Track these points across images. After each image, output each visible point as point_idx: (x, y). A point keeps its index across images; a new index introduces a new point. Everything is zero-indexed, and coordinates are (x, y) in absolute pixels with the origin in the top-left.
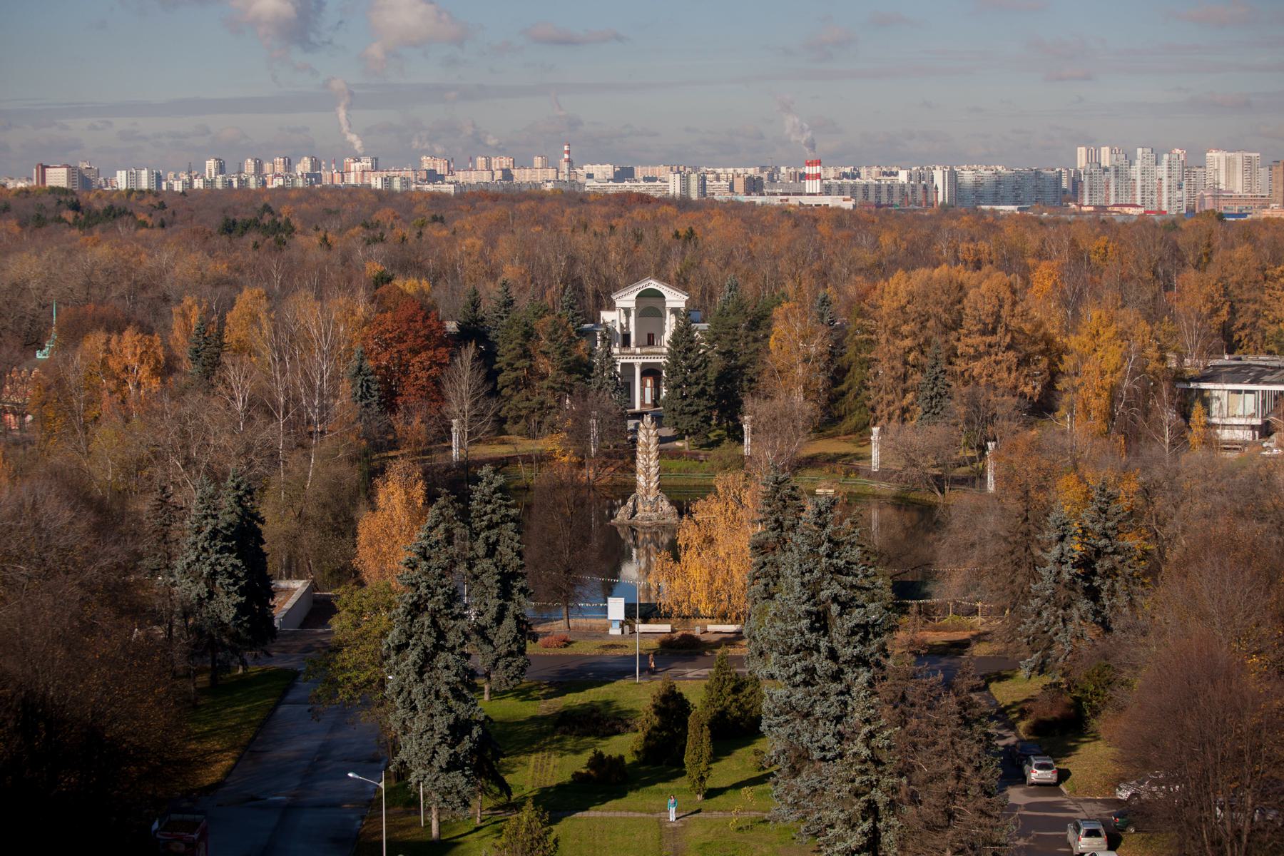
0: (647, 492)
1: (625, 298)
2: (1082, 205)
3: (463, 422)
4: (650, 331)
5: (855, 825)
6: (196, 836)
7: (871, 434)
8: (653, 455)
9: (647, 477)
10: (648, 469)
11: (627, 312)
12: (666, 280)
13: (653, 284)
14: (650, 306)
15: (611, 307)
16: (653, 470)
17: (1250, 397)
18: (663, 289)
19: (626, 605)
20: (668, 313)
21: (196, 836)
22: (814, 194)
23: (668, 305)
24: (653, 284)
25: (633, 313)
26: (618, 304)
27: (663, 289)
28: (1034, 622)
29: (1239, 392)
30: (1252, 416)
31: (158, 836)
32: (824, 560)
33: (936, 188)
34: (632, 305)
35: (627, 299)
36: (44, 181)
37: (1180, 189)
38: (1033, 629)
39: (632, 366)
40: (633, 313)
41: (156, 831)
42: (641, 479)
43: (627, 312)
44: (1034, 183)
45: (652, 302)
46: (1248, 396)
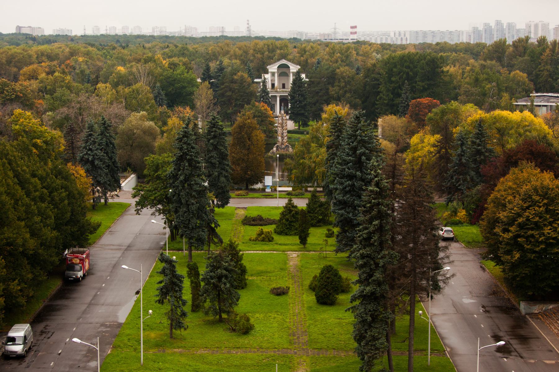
0: (282, 144)
1: (273, 68)
3: (203, 116)
5: (355, 93)
6: (84, 256)
9: (282, 137)
10: (282, 134)
11: (273, 74)
12: (289, 60)
15: (267, 72)
17: (544, 108)
18: (289, 64)
20: (291, 75)
21: (84, 256)
23: (291, 71)
24: (284, 62)
25: (276, 75)
26: (270, 70)
27: (289, 64)
28: (449, 181)
31: (67, 256)
33: (407, 39)
34: (276, 71)
35: (273, 68)
38: (449, 184)
39: (276, 97)
40: (276, 75)
41: (66, 254)
43: (273, 74)
44: (449, 36)
45: (284, 70)
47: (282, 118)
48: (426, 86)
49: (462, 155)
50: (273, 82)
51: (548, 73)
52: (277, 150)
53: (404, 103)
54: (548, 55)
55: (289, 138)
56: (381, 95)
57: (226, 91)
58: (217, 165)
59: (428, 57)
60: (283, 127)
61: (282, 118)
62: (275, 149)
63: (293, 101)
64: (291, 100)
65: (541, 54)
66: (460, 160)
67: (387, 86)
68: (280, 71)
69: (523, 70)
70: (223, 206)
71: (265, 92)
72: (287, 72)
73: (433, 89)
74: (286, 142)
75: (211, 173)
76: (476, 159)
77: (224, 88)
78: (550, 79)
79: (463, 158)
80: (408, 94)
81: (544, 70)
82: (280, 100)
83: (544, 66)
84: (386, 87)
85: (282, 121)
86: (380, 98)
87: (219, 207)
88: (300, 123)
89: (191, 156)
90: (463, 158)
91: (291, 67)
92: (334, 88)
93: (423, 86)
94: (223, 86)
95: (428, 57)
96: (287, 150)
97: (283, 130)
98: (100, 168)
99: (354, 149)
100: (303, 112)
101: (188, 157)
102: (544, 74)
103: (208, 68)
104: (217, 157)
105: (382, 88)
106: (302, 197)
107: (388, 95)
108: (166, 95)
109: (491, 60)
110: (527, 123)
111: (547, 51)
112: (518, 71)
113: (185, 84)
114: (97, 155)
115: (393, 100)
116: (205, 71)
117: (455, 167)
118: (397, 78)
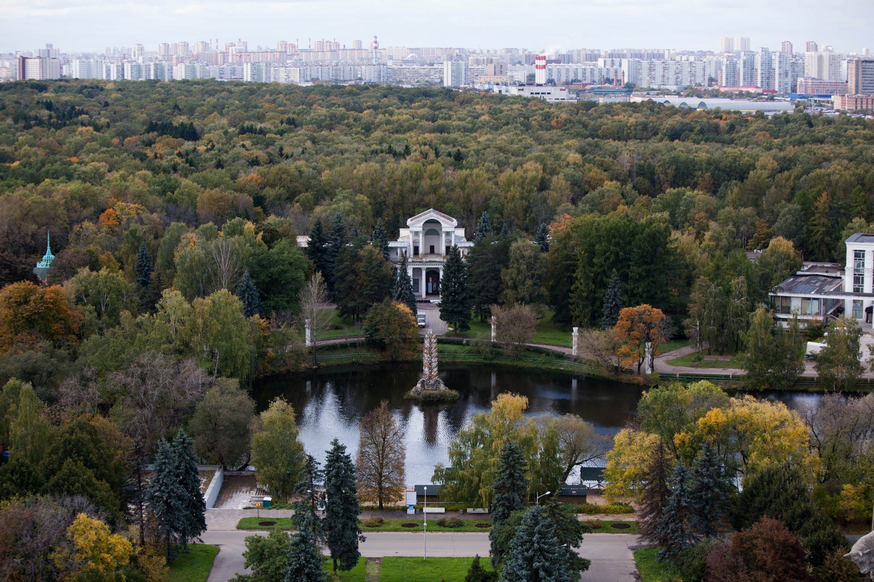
0: (430, 378)
2: (721, 86)
4: (432, 244)
7: (572, 331)
8: (435, 354)
9: (430, 369)
10: (430, 364)
13: (432, 214)
14: (432, 229)
16: (434, 364)
17: (816, 303)
19: (417, 496)
22: (541, 85)
23: (444, 230)
25: (421, 235)
29: (809, 299)
30: (818, 314)
32: (536, 545)
34: (421, 229)
35: (416, 224)
36: (24, 76)
37: (787, 76)
39: (420, 270)
42: (426, 359)
45: (433, 226)
46: (814, 301)
47: (430, 341)
48: (644, 274)
49: (681, 496)
50: (416, 245)
51: (824, 229)
52: (423, 386)
53: (612, 303)
54: (825, 203)
55: (440, 352)
56: (577, 283)
57: (346, 275)
58: (340, 515)
59: (647, 229)
60: (432, 353)
61: (430, 341)
62: (419, 385)
63: (446, 293)
64: (443, 291)
65: (815, 199)
66: (679, 501)
67: (587, 271)
68: (427, 229)
69: (788, 237)
70: (349, 567)
71: (405, 280)
72: (438, 229)
73: (653, 277)
74: (436, 376)
75: (333, 525)
76: (701, 496)
77: (343, 269)
78: (827, 239)
79: (683, 499)
80: (616, 290)
81: (819, 224)
82: (427, 274)
83: (819, 218)
84: (585, 272)
85: (430, 345)
86: (577, 288)
87: (343, 570)
88: (457, 326)
89: (310, 568)
90: (683, 499)
91: (443, 225)
92: (510, 271)
93: (640, 274)
94: (343, 266)
95: (647, 229)
96: (437, 388)
97: (432, 358)
98: (179, 510)
99: (530, 560)
100: (461, 309)
101: (307, 570)
102: (819, 231)
103: (319, 227)
104: (341, 503)
105: (579, 273)
106: (459, 529)
107: (588, 284)
108: (257, 284)
109: (745, 205)
110: (777, 423)
111: (823, 195)
112: (781, 238)
113: (286, 268)
114: (173, 492)
115: (595, 292)
116: (314, 232)
117: (672, 510)
118: (602, 260)
